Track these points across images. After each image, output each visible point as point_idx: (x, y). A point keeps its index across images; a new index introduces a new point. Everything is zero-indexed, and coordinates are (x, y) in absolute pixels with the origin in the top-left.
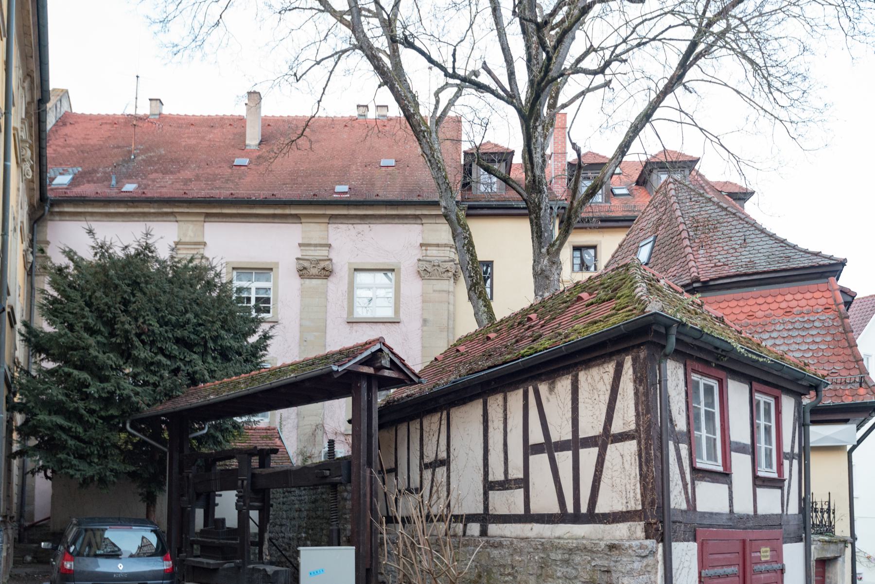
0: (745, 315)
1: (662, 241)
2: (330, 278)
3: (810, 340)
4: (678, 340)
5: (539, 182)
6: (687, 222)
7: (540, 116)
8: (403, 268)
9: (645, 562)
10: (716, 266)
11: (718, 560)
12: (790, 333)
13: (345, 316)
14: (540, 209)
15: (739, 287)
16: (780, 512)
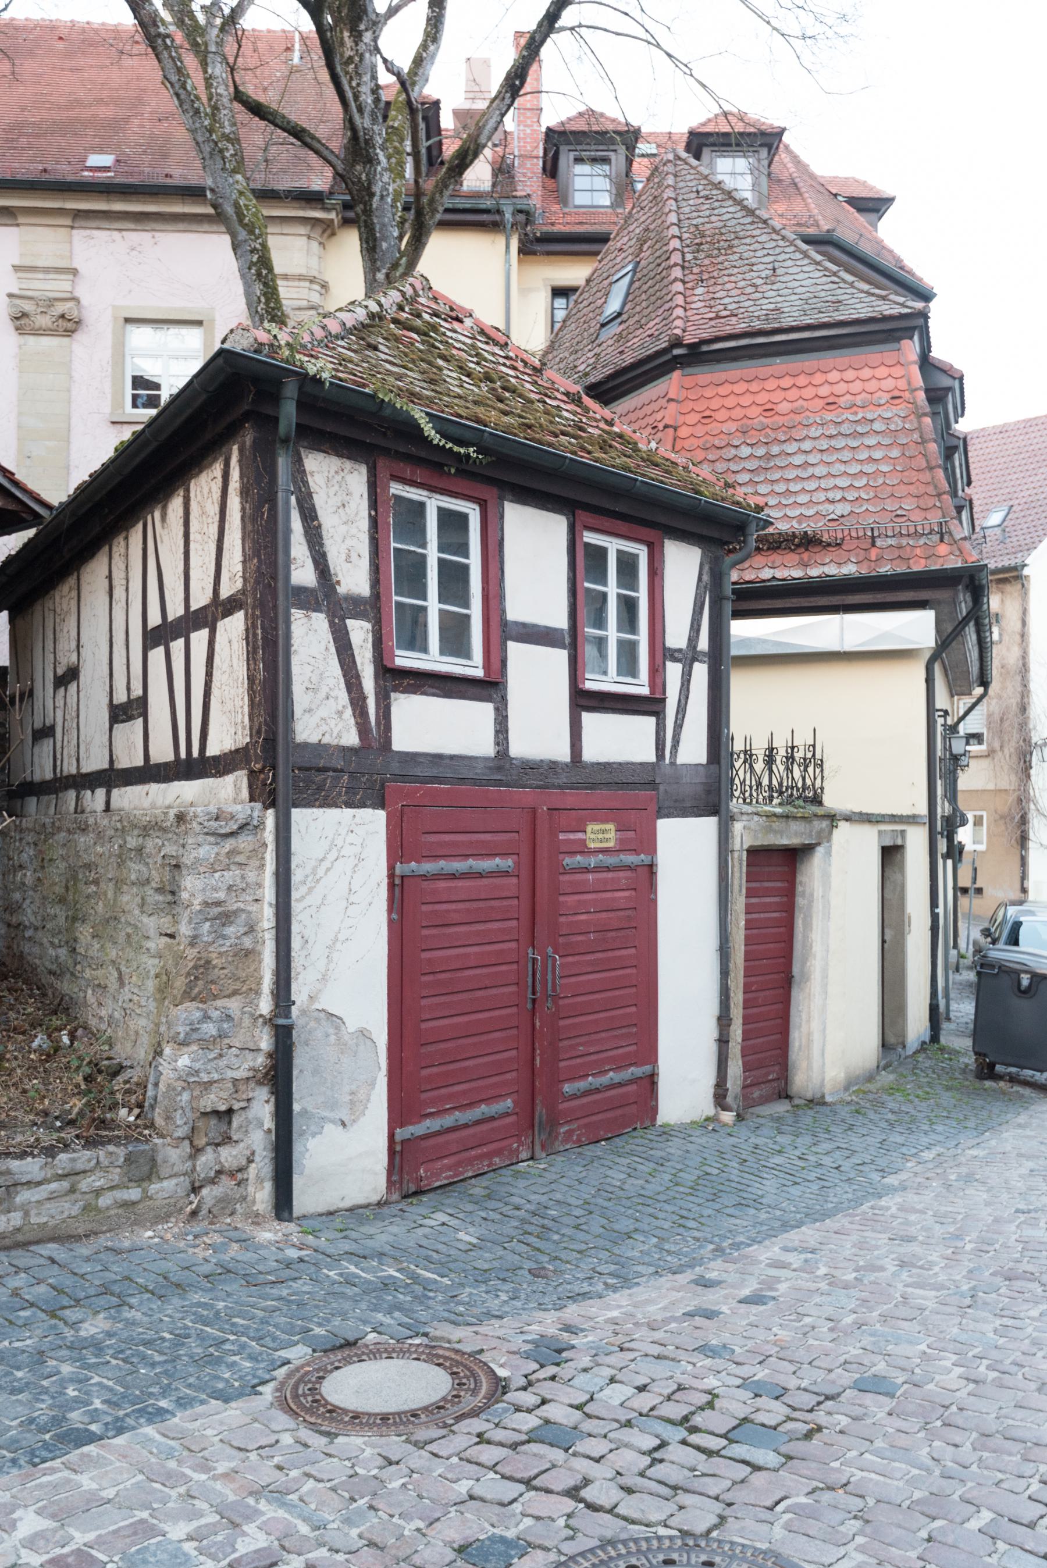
0: (760, 409)
1: (645, 271)
2: (77, 336)
3: (863, 455)
4: (301, 405)
5: (367, 142)
6: (685, 236)
7: (365, 12)
8: (217, 317)
9: (229, 844)
10: (718, 317)
11: (454, 844)
12: (833, 443)
13: (107, 410)
14: (372, 195)
15: (751, 357)
16: (653, 758)
